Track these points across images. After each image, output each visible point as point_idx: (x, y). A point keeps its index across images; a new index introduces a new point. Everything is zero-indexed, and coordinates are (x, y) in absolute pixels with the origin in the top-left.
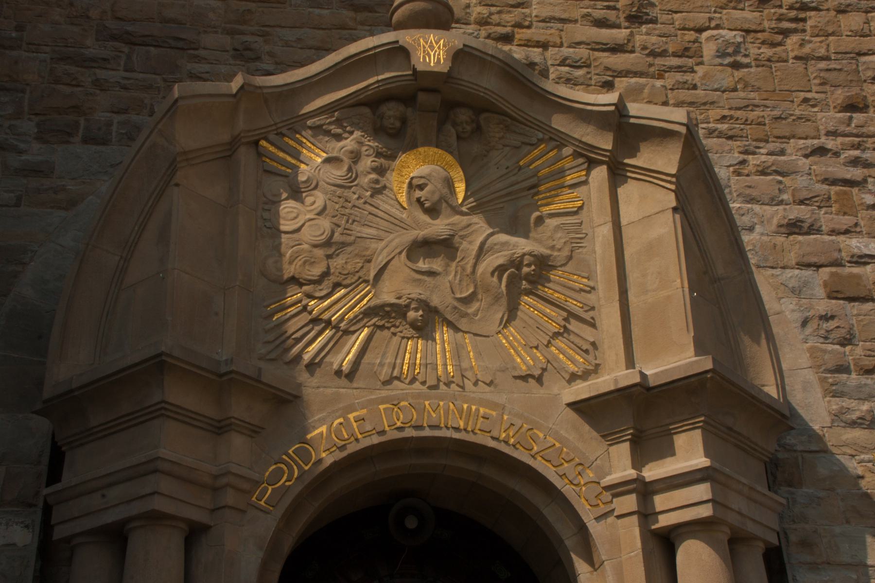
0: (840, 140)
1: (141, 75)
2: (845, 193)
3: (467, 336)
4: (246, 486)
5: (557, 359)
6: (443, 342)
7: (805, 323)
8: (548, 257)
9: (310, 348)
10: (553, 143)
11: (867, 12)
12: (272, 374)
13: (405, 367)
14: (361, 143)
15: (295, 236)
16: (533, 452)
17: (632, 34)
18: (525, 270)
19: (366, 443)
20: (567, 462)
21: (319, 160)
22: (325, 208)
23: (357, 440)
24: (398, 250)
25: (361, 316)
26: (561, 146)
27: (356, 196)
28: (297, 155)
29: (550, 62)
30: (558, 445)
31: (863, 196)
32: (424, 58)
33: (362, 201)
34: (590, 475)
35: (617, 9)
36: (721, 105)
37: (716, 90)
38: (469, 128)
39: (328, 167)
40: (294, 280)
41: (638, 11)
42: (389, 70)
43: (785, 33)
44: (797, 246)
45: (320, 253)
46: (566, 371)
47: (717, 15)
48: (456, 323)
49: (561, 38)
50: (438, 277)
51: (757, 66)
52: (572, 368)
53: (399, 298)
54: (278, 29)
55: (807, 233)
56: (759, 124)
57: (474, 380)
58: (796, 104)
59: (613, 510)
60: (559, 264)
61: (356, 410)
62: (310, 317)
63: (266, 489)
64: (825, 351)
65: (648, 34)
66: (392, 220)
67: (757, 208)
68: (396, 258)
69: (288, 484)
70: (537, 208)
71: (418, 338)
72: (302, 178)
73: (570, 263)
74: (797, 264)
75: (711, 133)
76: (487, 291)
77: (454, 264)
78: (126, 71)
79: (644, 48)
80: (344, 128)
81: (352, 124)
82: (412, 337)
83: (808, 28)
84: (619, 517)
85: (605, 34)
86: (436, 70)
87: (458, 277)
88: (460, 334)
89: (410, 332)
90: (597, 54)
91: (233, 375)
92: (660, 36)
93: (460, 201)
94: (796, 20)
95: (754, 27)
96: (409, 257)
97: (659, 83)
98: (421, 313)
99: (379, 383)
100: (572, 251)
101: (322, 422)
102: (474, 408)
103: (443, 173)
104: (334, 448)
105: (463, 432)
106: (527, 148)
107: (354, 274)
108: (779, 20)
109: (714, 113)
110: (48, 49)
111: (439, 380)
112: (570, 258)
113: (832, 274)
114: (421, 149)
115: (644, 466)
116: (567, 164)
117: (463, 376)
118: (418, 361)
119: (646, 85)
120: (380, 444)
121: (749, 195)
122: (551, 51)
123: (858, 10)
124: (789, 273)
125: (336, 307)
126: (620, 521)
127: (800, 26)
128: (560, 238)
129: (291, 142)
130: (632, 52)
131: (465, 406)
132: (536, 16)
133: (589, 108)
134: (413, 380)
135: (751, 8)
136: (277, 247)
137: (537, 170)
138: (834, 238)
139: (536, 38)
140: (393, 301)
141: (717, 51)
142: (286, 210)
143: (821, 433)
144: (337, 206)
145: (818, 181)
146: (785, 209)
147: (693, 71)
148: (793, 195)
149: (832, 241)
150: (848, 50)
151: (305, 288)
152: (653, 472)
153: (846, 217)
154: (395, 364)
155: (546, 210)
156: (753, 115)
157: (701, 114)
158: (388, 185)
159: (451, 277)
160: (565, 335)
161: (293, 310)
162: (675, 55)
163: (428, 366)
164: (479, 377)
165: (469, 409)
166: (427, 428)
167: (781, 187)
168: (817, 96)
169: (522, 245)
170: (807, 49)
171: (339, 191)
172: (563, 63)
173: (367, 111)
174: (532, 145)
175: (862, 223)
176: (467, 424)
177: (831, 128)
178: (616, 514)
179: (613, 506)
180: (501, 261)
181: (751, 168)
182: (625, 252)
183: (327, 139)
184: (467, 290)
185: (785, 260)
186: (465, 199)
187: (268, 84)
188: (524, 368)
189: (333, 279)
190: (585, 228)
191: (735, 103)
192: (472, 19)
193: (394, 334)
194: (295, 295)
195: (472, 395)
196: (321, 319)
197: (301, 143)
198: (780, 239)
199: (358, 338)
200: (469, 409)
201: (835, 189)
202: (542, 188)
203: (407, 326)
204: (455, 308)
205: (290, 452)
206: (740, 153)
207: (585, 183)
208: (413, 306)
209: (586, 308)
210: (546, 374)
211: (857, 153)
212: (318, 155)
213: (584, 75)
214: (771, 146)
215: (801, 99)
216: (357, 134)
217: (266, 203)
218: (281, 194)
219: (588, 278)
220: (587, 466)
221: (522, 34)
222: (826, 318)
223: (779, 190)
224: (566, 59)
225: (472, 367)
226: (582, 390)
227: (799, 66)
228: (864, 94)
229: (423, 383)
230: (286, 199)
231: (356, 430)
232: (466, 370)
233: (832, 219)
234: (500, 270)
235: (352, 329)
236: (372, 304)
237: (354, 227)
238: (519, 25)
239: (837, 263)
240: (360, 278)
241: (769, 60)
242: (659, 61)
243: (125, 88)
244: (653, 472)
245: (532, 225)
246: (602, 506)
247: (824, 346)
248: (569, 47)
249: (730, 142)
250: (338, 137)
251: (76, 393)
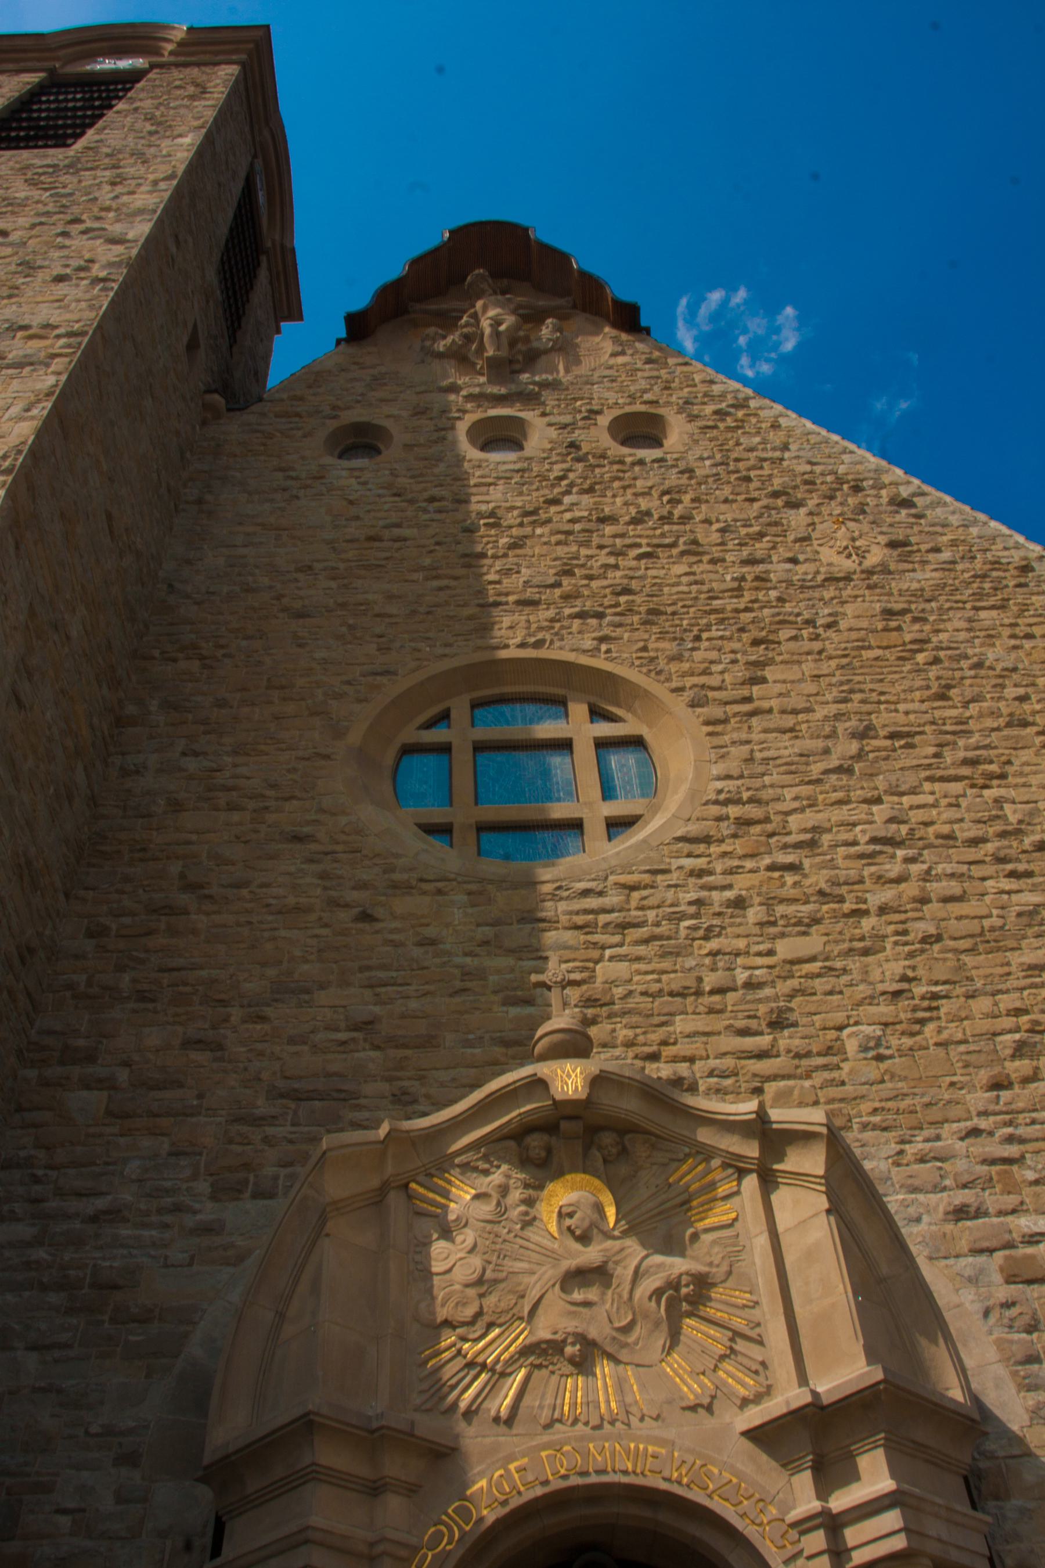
0: (992, 1119)
1: (306, 1129)
2: (1006, 1171)
3: (629, 1368)
4: (403, 1553)
5: (725, 1383)
6: (604, 1376)
7: (986, 1313)
8: (707, 1274)
9: (466, 1395)
10: (701, 1157)
11: (993, 995)
12: (426, 1426)
13: (566, 1408)
14: (508, 1177)
15: (447, 1276)
16: (709, 1491)
17: (775, 1039)
18: (684, 1291)
19: (529, 1495)
20: (747, 1499)
21: (468, 1197)
22: (475, 1245)
23: (519, 1493)
24: (551, 1283)
25: (517, 1356)
26: (708, 1159)
27: (506, 1230)
28: (446, 1195)
29: (698, 1075)
30: (735, 1480)
31: (1024, 1172)
32: (562, 1087)
33: (513, 1234)
34: (773, 1511)
35: (759, 1018)
36: (871, 1097)
37: (864, 1084)
38: (614, 1151)
39: (477, 1203)
40: (447, 1323)
41: (778, 1016)
42: (529, 1102)
43: (922, 1022)
44: (967, 1232)
45: (472, 1292)
46: (737, 1397)
47: (854, 1013)
48: (616, 1355)
49: (707, 1050)
50: (594, 1307)
51: (900, 1056)
52: (743, 1392)
53: (555, 1333)
54: (434, 1072)
55: (976, 1217)
56: (911, 1112)
57: (639, 1415)
58: (943, 1089)
59: (801, 1551)
60: (719, 1280)
61: (516, 1459)
62: (464, 1362)
63: (425, 1556)
64: (1011, 1342)
65: (790, 1037)
66: (544, 1251)
67: (921, 1197)
68: (550, 1291)
69: (449, 1547)
70: (691, 1224)
71: (578, 1374)
72: (452, 1217)
73: (730, 1278)
74: (970, 1251)
75: (865, 1126)
76: (646, 1316)
77: (610, 1292)
78: (293, 1125)
79: (789, 1051)
80: (491, 1163)
81: (499, 1159)
82: (572, 1374)
83: (942, 1015)
84: (810, 1558)
85: (749, 1043)
86: (575, 1097)
87: (615, 1305)
88: (622, 1366)
89: (568, 1368)
90: (743, 1062)
91: (384, 1431)
92: (802, 1038)
93: (611, 1225)
94: (930, 1009)
95: (891, 1020)
96: (563, 1289)
97: (807, 1084)
98: (578, 1347)
99: (540, 1428)
100: (731, 1266)
101: (481, 1475)
102: (641, 1446)
103: (592, 1199)
104: (496, 1504)
105: (632, 1475)
106: (675, 1164)
107: (507, 1311)
108: (915, 1009)
109: (866, 1107)
110: (223, 1113)
111: (602, 1419)
112: (729, 1273)
113: (1007, 1258)
114: (568, 1177)
115: (830, 1495)
116: (717, 1175)
117: (627, 1412)
118: (579, 1400)
119: (794, 1087)
120: (544, 1496)
121: (911, 1185)
122: (698, 1064)
123: (986, 994)
124: (963, 1262)
125: (491, 1348)
126: (810, 1563)
127: (935, 1014)
128: (717, 1253)
129: (440, 1182)
130: (778, 1056)
131: (632, 1445)
132: (681, 1033)
133: (732, 1118)
134: (576, 1421)
135: (887, 1002)
136: (430, 1290)
137: (688, 1186)
138: (1002, 1219)
139: (682, 1053)
140: (548, 1336)
141: (860, 1046)
142: (438, 1251)
143: (1019, 1433)
144: (487, 1243)
145: (977, 1163)
146: (949, 1196)
147: (839, 1068)
148: (955, 1180)
149: (1002, 1223)
150: (984, 1031)
151: (459, 1331)
152: (841, 1501)
153: (1011, 1196)
154: (555, 1405)
155: (700, 1225)
156: (903, 1104)
157: (853, 1109)
158: (538, 1216)
159: (608, 1306)
160: (733, 1356)
161: (447, 1355)
162: (819, 1054)
163: (591, 1405)
164: (645, 1411)
165: (637, 1448)
166: (593, 1474)
167: (942, 1173)
168: (962, 1079)
169: (678, 1265)
170: (945, 1035)
171: (489, 1227)
172: (711, 1074)
173: (512, 1144)
174: (680, 1160)
175: (1027, 1200)
176: (635, 1465)
177: (982, 1109)
178: (805, 1554)
179: (801, 1545)
180: (657, 1284)
181: (909, 1157)
182: (786, 1261)
183: (475, 1175)
184: (626, 1318)
185: (958, 1248)
186: (617, 1222)
187: (415, 1127)
188: (692, 1397)
189: (486, 1319)
190: (742, 1240)
191: (884, 1094)
192: (619, 1042)
193: (553, 1372)
194: (449, 1339)
195: (639, 1433)
196: (476, 1363)
197: (450, 1182)
198: (949, 1227)
199: (515, 1380)
200: (637, 1448)
201: (995, 1169)
202: (694, 1203)
203: (566, 1363)
204: (614, 1338)
205: (450, 1511)
206: (897, 1143)
207: (737, 1193)
208: (569, 1340)
209: (751, 1325)
210: (715, 1401)
211: (1009, 1130)
212: (467, 1192)
213: (733, 1084)
214: (927, 1133)
215: (947, 1083)
216: (505, 1167)
217: (417, 1246)
218: (431, 1235)
219: (751, 1293)
220: (768, 1500)
221: (668, 1051)
222: (1008, 1305)
223: (941, 1176)
224: (713, 1070)
225: (636, 1402)
226: (755, 1416)
227: (941, 1052)
228: (1006, 1071)
229: (586, 1424)
230: (438, 1239)
231: (518, 1482)
232: (630, 1405)
233: (998, 1200)
234: (658, 1293)
235: (509, 1370)
236: (528, 1342)
237: (506, 1262)
238: (664, 1043)
239: (1010, 1245)
240: (514, 1315)
241: (911, 1049)
242: (804, 1062)
243: (291, 1142)
244: (841, 1501)
245: (687, 1242)
246: (789, 1546)
247: (1010, 1336)
248: (716, 1058)
249: (885, 1134)
250: (486, 1173)
251: (233, 1458)
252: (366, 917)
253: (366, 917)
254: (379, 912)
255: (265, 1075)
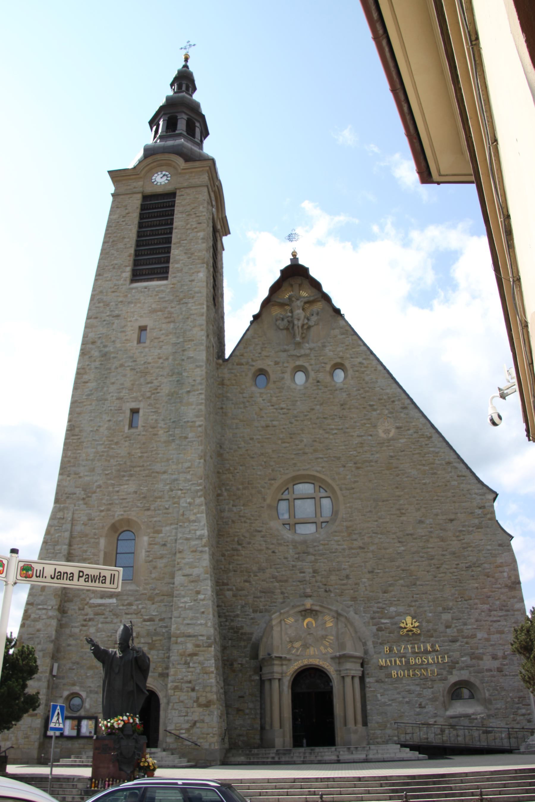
252: (274, 552)
253: (274, 552)
254: (276, 551)
255: (259, 588)
